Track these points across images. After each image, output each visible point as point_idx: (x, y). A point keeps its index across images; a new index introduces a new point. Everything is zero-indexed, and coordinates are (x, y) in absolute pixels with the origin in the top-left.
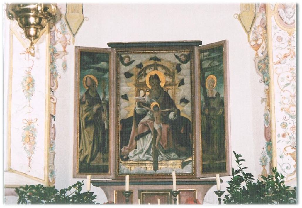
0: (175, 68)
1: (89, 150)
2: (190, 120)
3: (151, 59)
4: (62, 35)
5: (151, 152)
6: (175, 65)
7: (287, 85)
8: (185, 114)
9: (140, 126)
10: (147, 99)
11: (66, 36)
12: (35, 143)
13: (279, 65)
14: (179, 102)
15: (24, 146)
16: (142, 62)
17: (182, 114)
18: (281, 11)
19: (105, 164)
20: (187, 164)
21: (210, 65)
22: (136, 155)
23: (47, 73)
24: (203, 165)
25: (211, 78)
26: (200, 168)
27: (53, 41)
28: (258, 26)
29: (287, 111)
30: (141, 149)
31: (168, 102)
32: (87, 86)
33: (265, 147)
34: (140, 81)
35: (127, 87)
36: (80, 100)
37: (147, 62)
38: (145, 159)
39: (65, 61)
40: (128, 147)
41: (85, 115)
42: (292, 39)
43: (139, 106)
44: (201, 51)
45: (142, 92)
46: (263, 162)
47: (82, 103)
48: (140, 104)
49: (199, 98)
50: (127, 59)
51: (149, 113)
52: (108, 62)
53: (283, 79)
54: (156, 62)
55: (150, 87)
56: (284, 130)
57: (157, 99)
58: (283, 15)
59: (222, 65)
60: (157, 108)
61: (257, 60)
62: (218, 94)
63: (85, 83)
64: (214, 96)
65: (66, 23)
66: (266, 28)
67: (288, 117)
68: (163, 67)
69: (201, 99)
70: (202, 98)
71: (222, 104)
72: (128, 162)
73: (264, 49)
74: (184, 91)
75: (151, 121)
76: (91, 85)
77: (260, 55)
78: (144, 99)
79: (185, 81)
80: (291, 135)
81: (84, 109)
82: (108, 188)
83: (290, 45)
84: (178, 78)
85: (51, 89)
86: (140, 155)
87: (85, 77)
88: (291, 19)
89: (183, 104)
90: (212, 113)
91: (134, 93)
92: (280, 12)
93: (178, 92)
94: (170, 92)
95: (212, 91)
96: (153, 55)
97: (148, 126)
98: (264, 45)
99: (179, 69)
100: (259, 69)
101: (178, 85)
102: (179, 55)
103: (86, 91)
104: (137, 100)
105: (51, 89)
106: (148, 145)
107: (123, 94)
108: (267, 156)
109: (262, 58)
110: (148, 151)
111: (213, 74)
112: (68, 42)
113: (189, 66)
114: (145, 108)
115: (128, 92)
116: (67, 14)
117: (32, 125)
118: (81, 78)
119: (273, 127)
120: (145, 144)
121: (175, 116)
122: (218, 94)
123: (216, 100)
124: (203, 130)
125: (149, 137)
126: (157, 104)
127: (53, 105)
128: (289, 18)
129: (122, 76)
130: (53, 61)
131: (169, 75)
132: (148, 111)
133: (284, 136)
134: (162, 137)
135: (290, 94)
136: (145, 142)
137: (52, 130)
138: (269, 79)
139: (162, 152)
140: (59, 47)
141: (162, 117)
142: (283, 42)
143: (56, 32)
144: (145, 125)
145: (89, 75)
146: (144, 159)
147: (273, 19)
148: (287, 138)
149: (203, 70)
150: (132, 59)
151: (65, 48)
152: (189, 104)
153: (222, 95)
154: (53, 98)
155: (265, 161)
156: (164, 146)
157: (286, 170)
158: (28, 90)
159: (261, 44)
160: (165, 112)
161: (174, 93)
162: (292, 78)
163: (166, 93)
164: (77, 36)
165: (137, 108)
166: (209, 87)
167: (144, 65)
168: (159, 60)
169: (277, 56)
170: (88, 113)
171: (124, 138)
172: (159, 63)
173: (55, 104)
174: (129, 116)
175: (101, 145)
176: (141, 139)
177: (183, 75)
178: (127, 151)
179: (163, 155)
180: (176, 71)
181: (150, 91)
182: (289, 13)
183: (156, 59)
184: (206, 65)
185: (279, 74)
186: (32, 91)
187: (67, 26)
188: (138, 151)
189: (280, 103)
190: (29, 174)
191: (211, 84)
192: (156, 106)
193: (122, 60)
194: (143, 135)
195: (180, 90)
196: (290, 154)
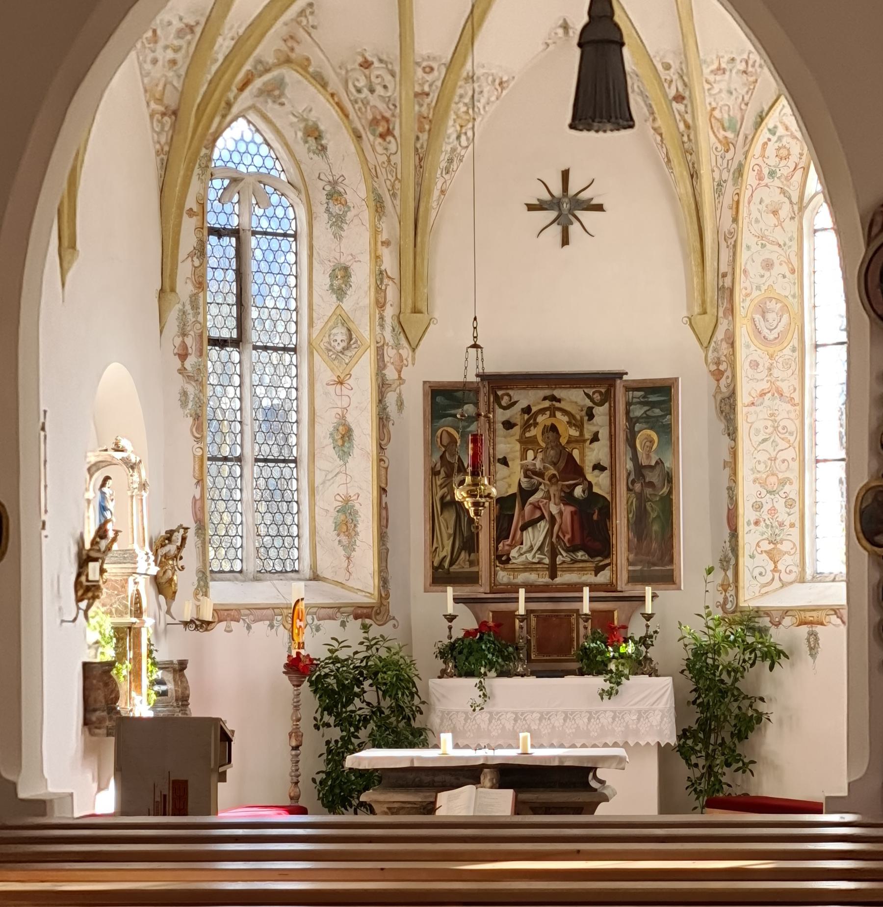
0: (584, 413)
1: (448, 548)
2: (609, 498)
3: (545, 399)
4: (395, 351)
5: (546, 549)
6: (585, 409)
7: (764, 440)
8: (600, 488)
9: (527, 508)
10: (539, 465)
11: (401, 351)
12: (357, 534)
13: (753, 409)
14: (591, 469)
15: (338, 538)
16: (531, 403)
17: (595, 490)
18: (758, 317)
19: (474, 569)
20: (603, 570)
21: (645, 412)
22: (522, 554)
23: (374, 418)
24: (629, 571)
25: (646, 434)
26: (623, 576)
27: (381, 364)
28: (722, 340)
29: (763, 484)
30: (529, 544)
31: (573, 470)
32: (443, 446)
33: (727, 539)
34: (528, 435)
35: (507, 445)
36: (433, 469)
37: (539, 403)
38: (536, 560)
39: (400, 395)
40: (508, 542)
41: (440, 494)
42: (775, 365)
43: (526, 476)
44: (628, 389)
45: (531, 454)
46: (725, 564)
47: (435, 473)
48: (529, 472)
49: (625, 465)
50: (506, 398)
51: (542, 487)
52: (476, 404)
53: (758, 431)
54: (554, 404)
55: (543, 445)
56: (758, 513)
57: (554, 464)
58: (761, 325)
59: (668, 417)
60: (554, 480)
61: (719, 398)
62: (659, 463)
63: (439, 440)
64: (653, 463)
65: (400, 330)
66: (732, 345)
67: (764, 492)
68: (564, 412)
69: (628, 467)
70: (630, 465)
71: (669, 478)
72: (510, 566)
73: (729, 381)
74: (598, 453)
75: (545, 501)
76: (448, 444)
77: (724, 389)
78: (535, 465)
79: (600, 436)
80: (768, 522)
81: (439, 483)
82: (478, 606)
83: (771, 374)
84: (589, 430)
85: (380, 444)
86: (528, 555)
87: (440, 432)
88: (773, 332)
89: (597, 472)
90: (648, 491)
91: (518, 454)
92: (756, 319)
93: (589, 453)
94: (576, 454)
95: (648, 456)
96: (547, 392)
97: (540, 508)
98: (728, 373)
99: (591, 416)
100: (722, 412)
101: (589, 442)
102: (590, 392)
103: (441, 453)
104: (522, 466)
105: (380, 444)
106: (541, 538)
107: (501, 457)
108: (730, 555)
109: (727, 395)
110: (540, 549)
111: (651, 428)
112: (405, 362)
113: (607, 411)
114: (536, 479)
115: (508, 453)
116: (401, 315)
117: (350, 503)
118: (434, 432)
119: (740, 511)
120: (535, 536)
121: (584, 492)
122: (659, 463)
123: (657, 471)
124: (630, 516)
125: (543, 526)
126: (555, 472)
127: (383, 472)
128: (771, 330)
129: (499, 426)
130: (382, 396)
131: (575, 425)
132: (540, 484)
133: (757, 523)
134: (563, 526)
135: (768, 456)
136: (536, 533)
137: (384, 512)
138: (735, 430)
139: (563, 549)
140: (391, 373)
141: (563, 494)
142: (759, 370)
143: (386, 347)
144: (536, 507)
145: (445, 428)
146: (534, 561)
147: (744, 330)
148: (762, 527)
149: (632, 421)
150: (514, 399)
151: (399, 372)
152: (607, 473)
153: (667, 465)
154: (383, 460)
155: (728, 562)
156: (566, 540)
157: (758, 577)
158: (343, 445)
159: (726, 371)
160: (568, 486)
161: (582, 455)
162: (772, 429)
163: (570, 456)
164: (418, 351)
165: (524, 480)
166: (643, 449)
167: (534, 409)
168: (559, 401)
169: (750, 394)
170: (445, 490)
171: (503, 530)
172: (557, 405)
173: (387, 469)
174: (511, 492)
175: (468, 542)
176: (530, 529)
177: (597, 425)
178: (507, 548)
179: (564, 554)
180: (586, 418)
181: (544, 451)
182: (771, 321)
183: (553, 398)
184: (638, 411)
185: (752, 423)
186: (349, 448)
187: (402, 335)
188: (525, 548)
189: (752, 470)
190: (349, 584)
191: (648, 444)
192: (554, 475)
193: (498, 399)
194: (533, 523)
195: (593, 450)
196: (766, 552)
